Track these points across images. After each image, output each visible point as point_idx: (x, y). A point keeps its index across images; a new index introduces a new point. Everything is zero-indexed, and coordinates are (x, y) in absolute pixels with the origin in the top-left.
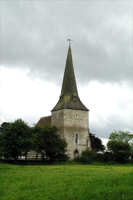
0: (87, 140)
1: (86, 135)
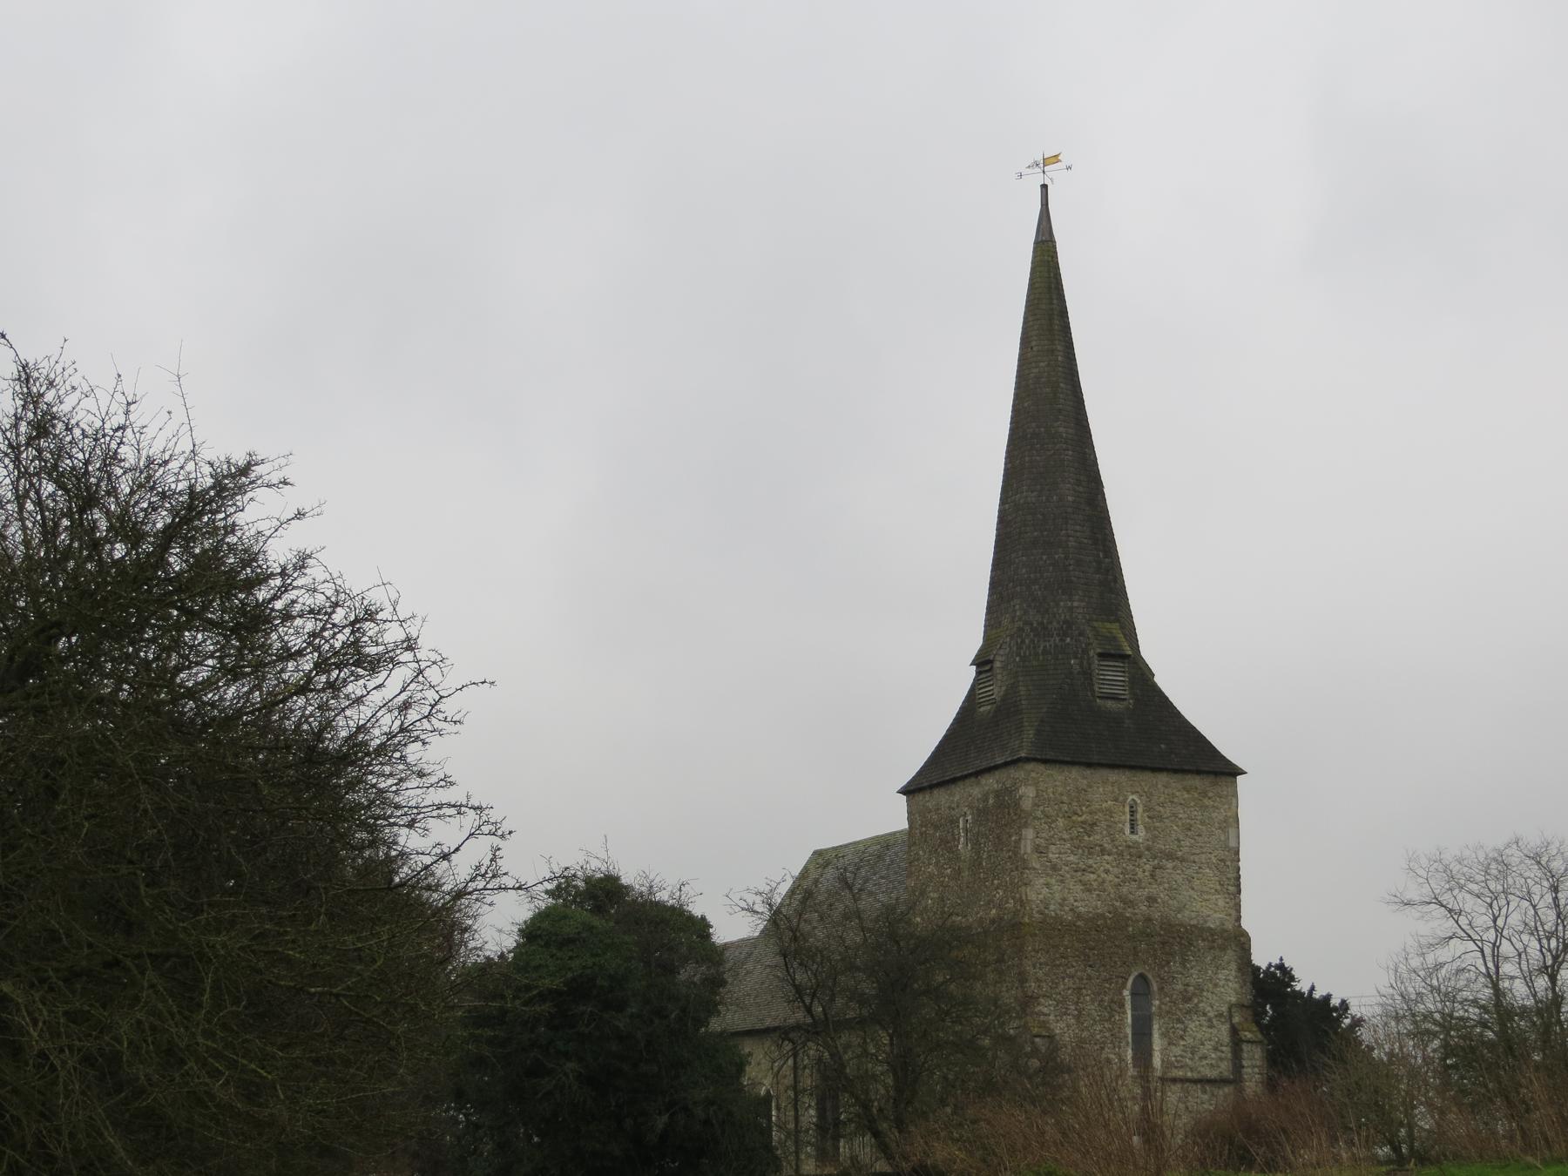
0: (1234, 1031)
1: (1227, 990)
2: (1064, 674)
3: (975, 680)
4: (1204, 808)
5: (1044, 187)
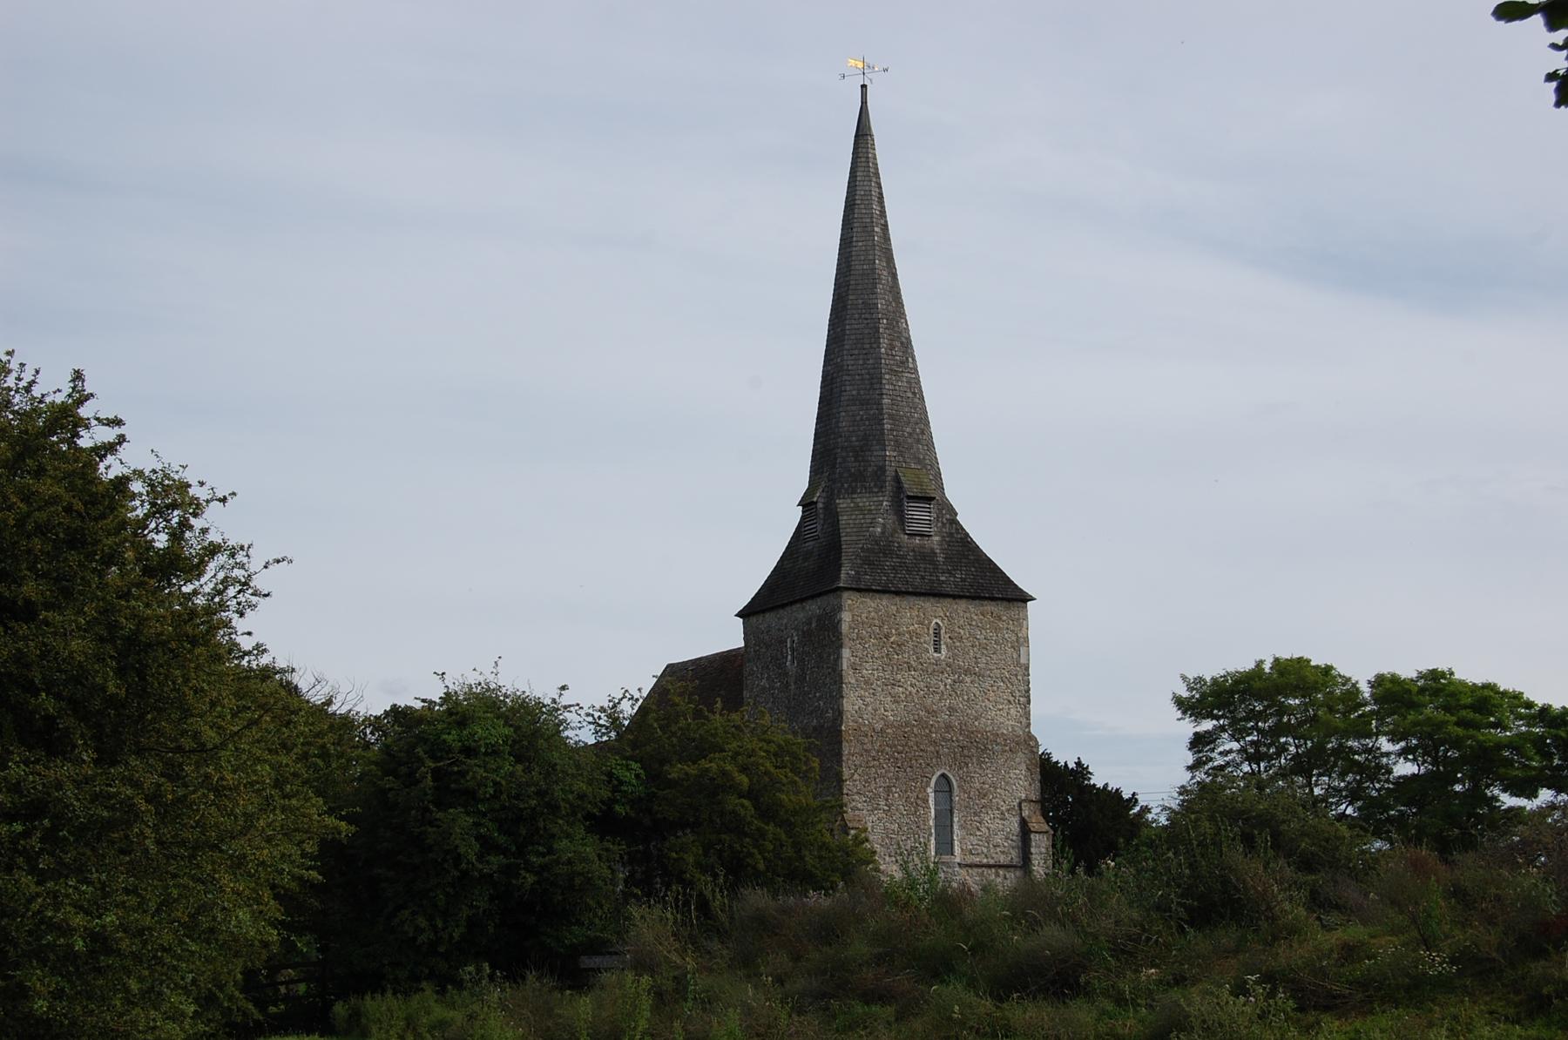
0: (1024, 823)
1: (1020, 785)
2: (875, 515)
3: (803, 518)
4: (997, 630)
5: (864, 87)
